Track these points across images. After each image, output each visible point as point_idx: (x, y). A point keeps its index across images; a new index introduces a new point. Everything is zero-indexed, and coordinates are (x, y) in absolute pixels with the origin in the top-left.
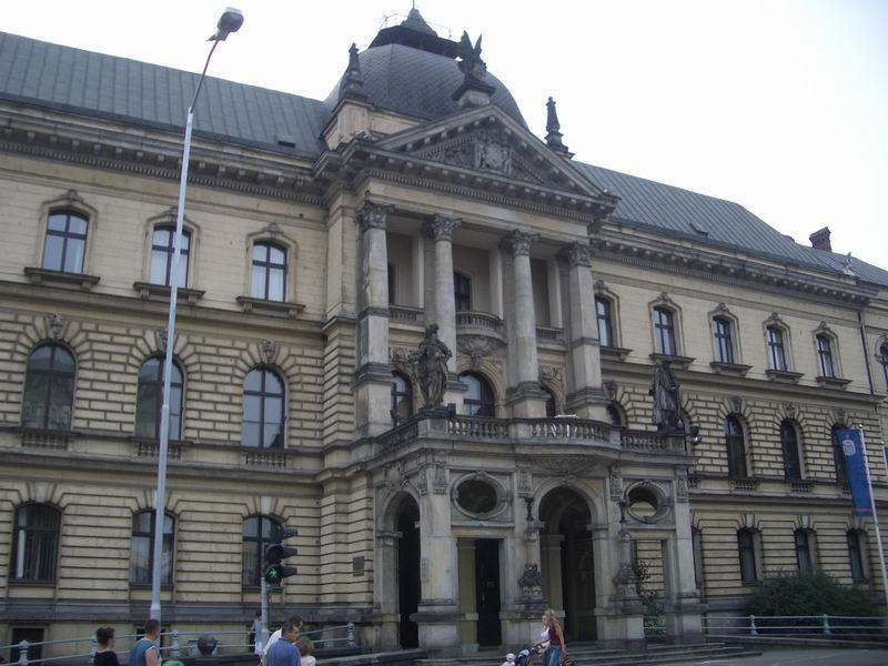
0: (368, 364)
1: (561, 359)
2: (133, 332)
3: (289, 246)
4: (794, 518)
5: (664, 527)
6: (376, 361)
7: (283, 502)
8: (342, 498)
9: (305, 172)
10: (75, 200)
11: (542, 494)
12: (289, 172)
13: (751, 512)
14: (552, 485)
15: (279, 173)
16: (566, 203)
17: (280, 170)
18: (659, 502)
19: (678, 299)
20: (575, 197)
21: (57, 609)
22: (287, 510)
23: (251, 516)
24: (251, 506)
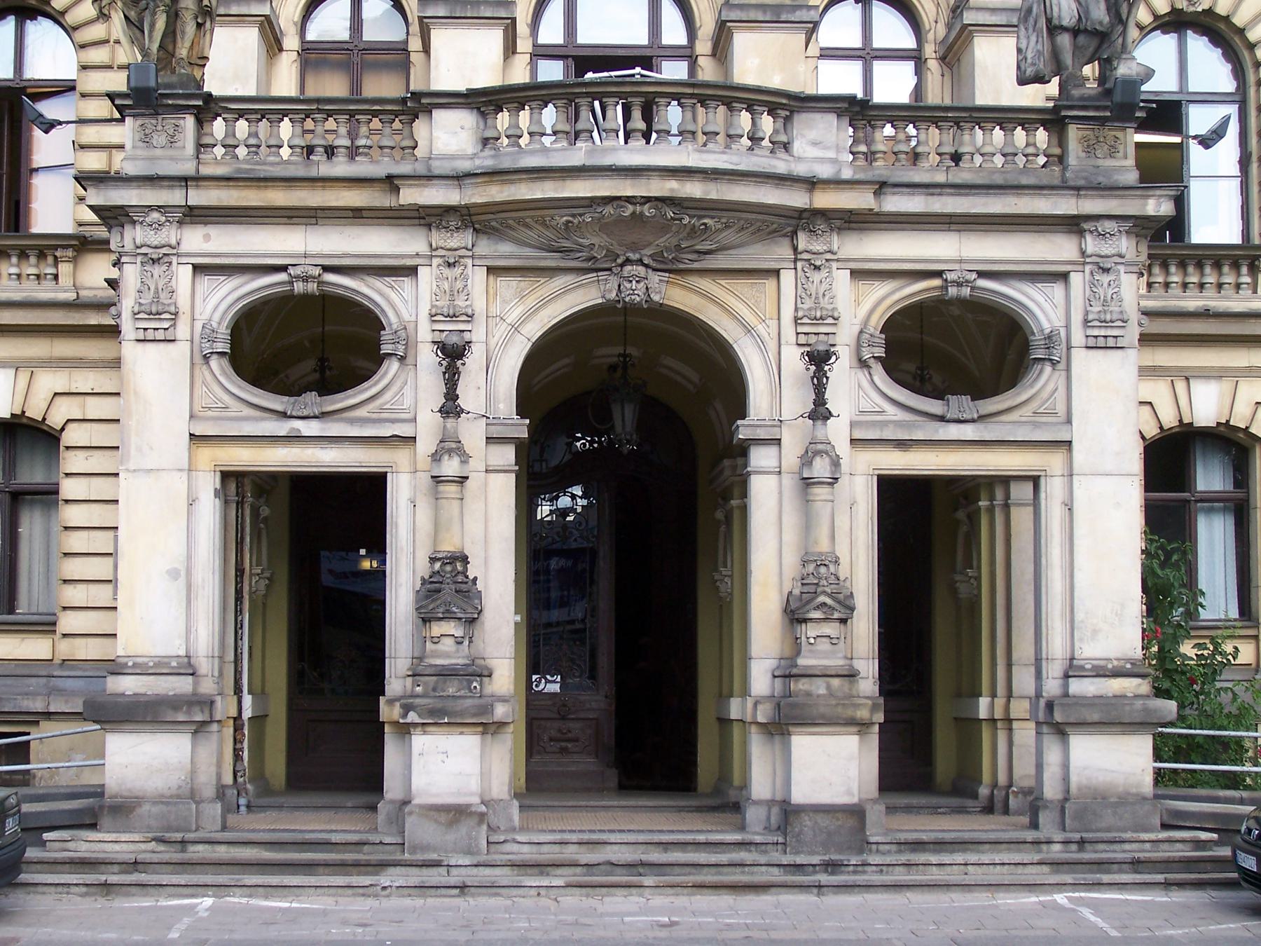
7: (49, 382)
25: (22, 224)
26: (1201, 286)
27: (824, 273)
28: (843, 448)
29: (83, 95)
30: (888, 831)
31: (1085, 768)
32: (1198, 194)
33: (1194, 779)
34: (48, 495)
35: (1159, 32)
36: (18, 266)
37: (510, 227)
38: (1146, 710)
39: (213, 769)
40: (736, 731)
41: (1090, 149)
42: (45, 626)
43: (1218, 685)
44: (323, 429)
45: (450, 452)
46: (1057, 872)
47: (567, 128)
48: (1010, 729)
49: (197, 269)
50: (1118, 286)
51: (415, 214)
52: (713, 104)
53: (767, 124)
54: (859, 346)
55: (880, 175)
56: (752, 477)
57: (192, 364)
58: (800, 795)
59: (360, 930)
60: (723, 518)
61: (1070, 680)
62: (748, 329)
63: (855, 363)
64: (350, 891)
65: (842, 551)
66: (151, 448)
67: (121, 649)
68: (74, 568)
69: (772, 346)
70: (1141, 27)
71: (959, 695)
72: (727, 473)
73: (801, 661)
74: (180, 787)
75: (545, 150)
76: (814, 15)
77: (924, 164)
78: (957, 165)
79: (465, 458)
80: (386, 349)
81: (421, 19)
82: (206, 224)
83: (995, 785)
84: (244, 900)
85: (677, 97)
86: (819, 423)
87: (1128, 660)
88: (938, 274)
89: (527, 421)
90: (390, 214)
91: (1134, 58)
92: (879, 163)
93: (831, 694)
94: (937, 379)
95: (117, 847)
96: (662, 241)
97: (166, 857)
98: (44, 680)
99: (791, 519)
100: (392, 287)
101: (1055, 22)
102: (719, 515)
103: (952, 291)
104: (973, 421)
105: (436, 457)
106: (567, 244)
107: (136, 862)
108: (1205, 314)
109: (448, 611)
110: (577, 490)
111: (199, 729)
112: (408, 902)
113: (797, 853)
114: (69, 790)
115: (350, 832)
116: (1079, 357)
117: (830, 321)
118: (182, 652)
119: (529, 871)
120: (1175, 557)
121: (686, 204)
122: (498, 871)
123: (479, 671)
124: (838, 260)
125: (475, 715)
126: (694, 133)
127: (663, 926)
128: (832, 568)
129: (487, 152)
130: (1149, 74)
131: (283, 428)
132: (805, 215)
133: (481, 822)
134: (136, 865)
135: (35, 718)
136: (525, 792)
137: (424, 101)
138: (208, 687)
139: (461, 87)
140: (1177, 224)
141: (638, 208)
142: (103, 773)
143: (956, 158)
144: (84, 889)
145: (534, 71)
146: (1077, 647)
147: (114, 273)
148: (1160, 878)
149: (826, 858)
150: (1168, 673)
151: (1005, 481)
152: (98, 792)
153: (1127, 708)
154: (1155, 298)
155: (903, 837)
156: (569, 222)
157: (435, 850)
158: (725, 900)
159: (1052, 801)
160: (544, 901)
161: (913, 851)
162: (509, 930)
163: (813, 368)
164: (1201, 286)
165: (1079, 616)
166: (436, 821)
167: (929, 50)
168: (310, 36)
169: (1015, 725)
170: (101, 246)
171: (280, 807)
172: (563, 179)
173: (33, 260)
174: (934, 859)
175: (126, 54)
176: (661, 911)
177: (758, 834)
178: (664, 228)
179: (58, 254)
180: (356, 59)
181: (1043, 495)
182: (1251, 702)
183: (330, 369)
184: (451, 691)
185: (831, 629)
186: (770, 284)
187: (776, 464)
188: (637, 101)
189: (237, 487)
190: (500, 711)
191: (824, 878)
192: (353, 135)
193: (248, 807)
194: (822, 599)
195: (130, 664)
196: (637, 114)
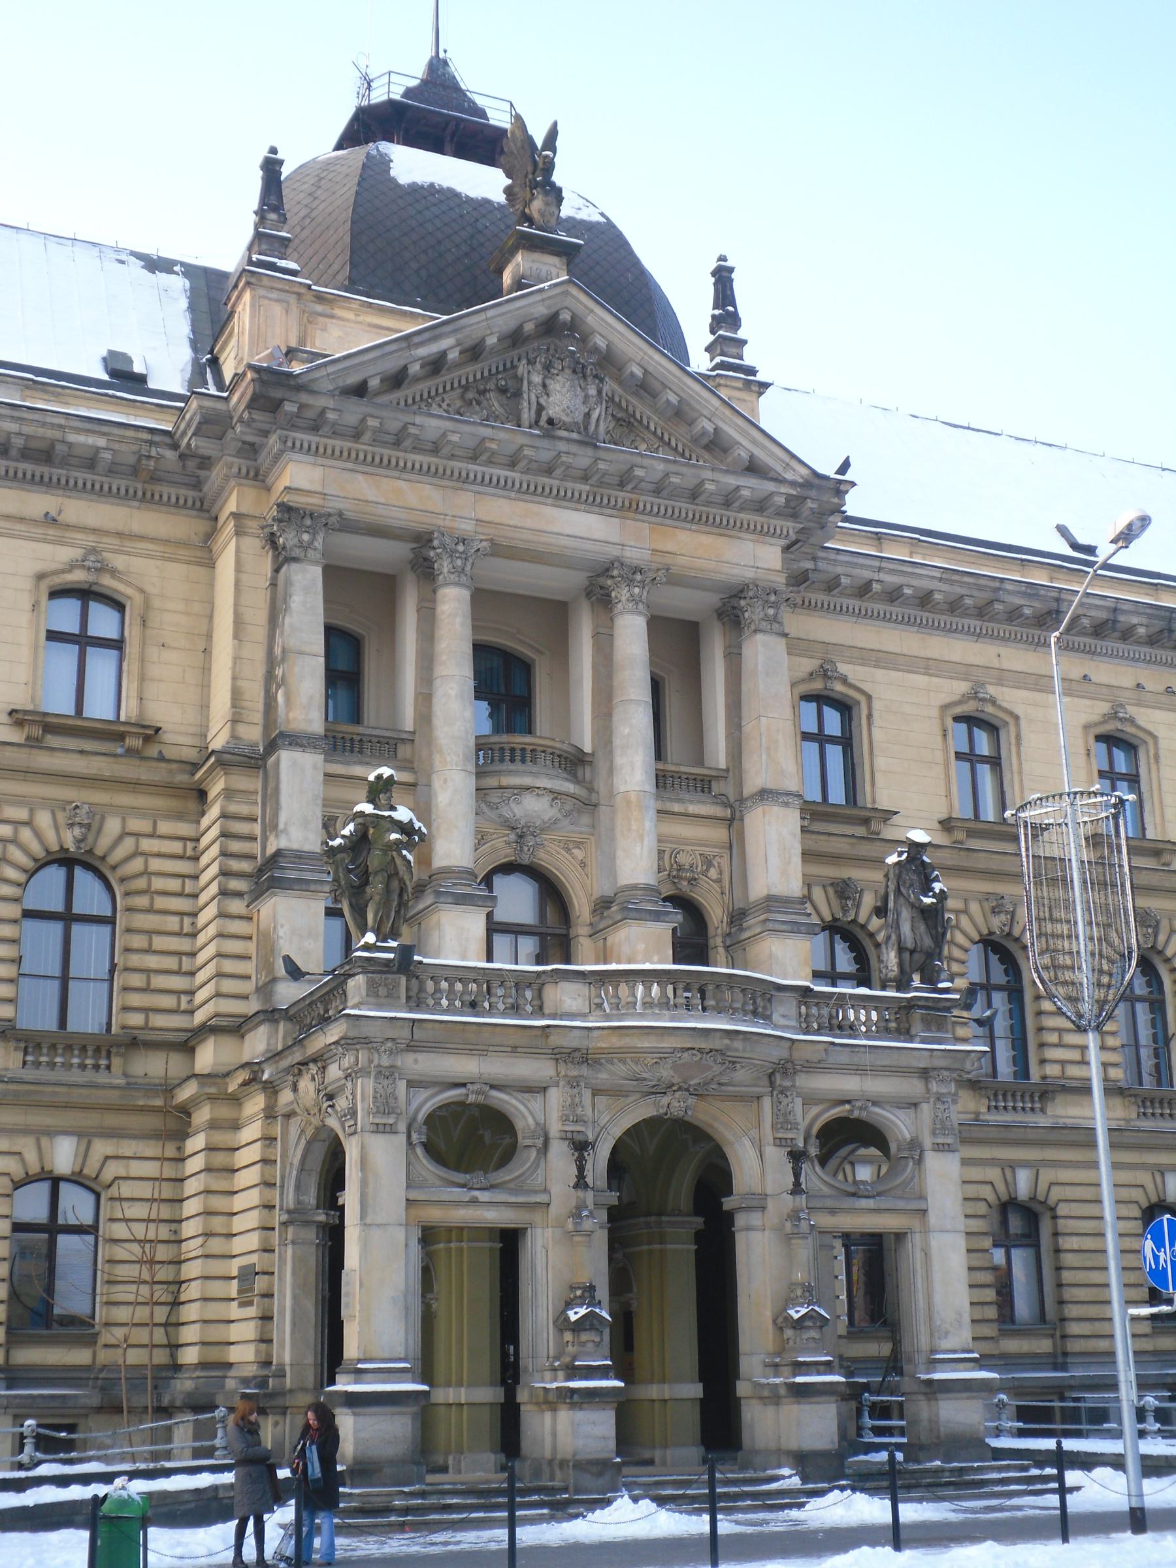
0: (278, 853)
5: (901, 1204)
6: (295, 846)
7: (101, 1148)
8: (221, 1138)
11: (617, 1131)
12: (122, 440)
13: (1026, 1164)
15: (101, 442)
18: (893, 1148)
19: (1011, 698)
20: (750, 487)
23: (29, 1180)
24: (31, 1157)
49: (411, 1084)
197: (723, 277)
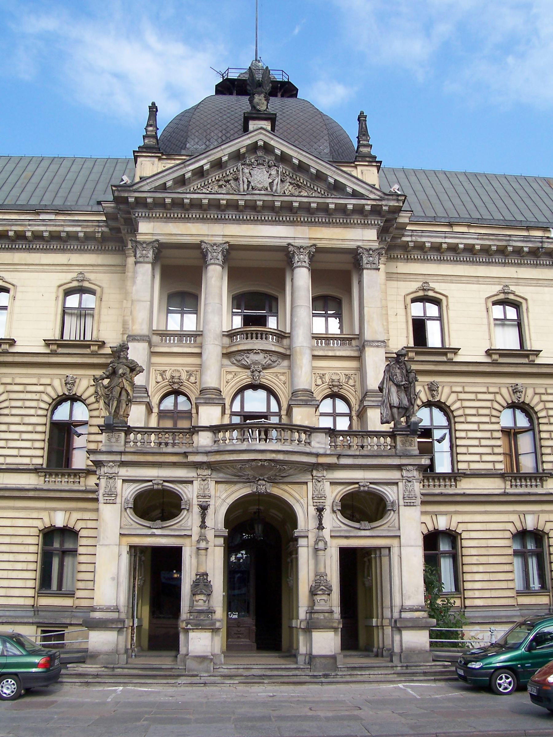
1: (354, 364)
2: (491, 390)
3: (521, 303)
4: (514, 518)
7: (76, 515)
9: (101, 224)
10: (509, 293)
12: (87, 226)
14: (242, 491)
15: (79, 229)
16: (342, 210)
17: (80, 226)
19: (520, 290)
20: (351, 203)
21: (467, 614)
22: (460, 525)
25: (69, 465)
26: (440, 486)
27: (321, 483)
28: (328, 538)
29: (90, 426)
30: (344, 664)
31: (408, 642)
32: (438, 457)
33: (443, 644)
34: (74, 552)
35: (424, 407)
36: (68, 478)
37: (222, 469)
38: (426, 622)
39: (124, 644)
40: (295, 630)
41: (403, 444)
42: (71, 595)
43: (449, 613)
44: (162, 532)
45: (203, 540)
46: (400, 676)
47: (241, 438)
48: (383, 629)
49: (124, 481)
50: (413, 486)
51: (193, 464)
52: (287, 430)
53: (303, 436)
54: (333, 506)
55: (339, 453)
56: (299, 548)
57: (121, 511)
58: (315, 652)
59: (171, 698)
60: (290, 561)
61: (402, 613)
62: (298, 501)
63: (332, 512)
64: (168, 685)
65: (328, 572)
66: (107, 538)
67: (95, 603)
68: (81, 576)
69: (305, 506)
70: (418, 406)
71: (366, 618)
72: (291, 546)
73: (315, 608)
74: (113, 649)
75: (234, 444)
76: (318, 403)
77: (352, 449)
78: (363, 449)
79: (207, 541)
80: (183, 507)
81: (196, 403)
82: (127, 466)
83: (378, 648)
84: (133, 688)
85: (275, 428)
86: (320, 531)
87: (420, 606)
88: (357, 483)
89: (227, 530)
90: (185, 464)
91: (416, 416)
92: (338, 449)
93: (325, 618)
94: (358, 516)
95: (91, 669)
96: (271, 473)
97: (107, 673)
98: (70, 613)
99: (312, 562)
100: (185, 487)
101: (392, 405)
102: (289, 560)
103: (362, 488)
104: (369, 530)
105: (198, 542)
106: (240, 474)
107: (97, 675)
108: (441, 494)
109: (202, 592)
110: (244, 552)
111: (120, 630)
112: (187, 689)
113: (314, 671)
114: (76, 650)
115: (168, 665)
116: (402, 509)
117: (324, 498)
118: (115, 605)
119: (227, 678)
120: (434, 572)
121: (278, 461)
122: (216, 678)
123: (211, 611)
124: (326, 479)
125: (210, 626)
126: (280, 440)
127: (271, 696)
128: (325, 578)
129: (216, 445)
130: (421, 420)
131: (149, 532)
132: (316, 465)
133: (211, 662)
134: (97, 676)
135: (66, 625)
136: (225, 650)
137: (196, 429)
138: (123, 616)
139: (208, 425)
140: (431, 467)
141: (263, 463)
142: (88, 644)
143: (362, 447)
144: (80, 684)
145: (231, 420)
146: (404, 602)
147: (98, 482)
148: (433, 678)
149: (324, 673)
150: (433, 610)
151: (380, 548)
152: (86, 651)
153: (420, 622)
154: (425, 490)
155: (349, 666)
156: (241, 467)
157: (196, 671)
158: (291, 687)
159: (397, 653)
160: (231, 688)
161: (352, 670)
162: (220, 698)
163: (318, 513)
164: (440, 486)
165: (404, 592)
166: (197, 661)
167: (354, 413)
168: (161, 408)
169: (385, 628)
170: (94, 473)
171: (146, 656)
172: (240, 453)
173: (72, 477)
174: (359, 673)
175: (104, 413)
176: (269, 692)
177: (302, 665)
178: (271, 469)
179: (80, 475)
180: (175, 415)
181: (392, 553)
182: (460, 619)
183: (165, 513)
184: (202, 618)
185: (325, 597)
186: (305, 487)
187: (307, 544)
188: (262, 429)
189: (134, 551)
190: (218, 625)
191: (323, 680)
192: (174, 439)
193: (135, 656)
194: (322, 587)
195: (98, 608)
196: (263, 433)
197: (362, 119)
